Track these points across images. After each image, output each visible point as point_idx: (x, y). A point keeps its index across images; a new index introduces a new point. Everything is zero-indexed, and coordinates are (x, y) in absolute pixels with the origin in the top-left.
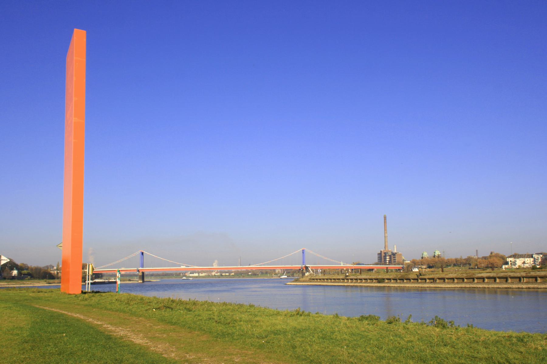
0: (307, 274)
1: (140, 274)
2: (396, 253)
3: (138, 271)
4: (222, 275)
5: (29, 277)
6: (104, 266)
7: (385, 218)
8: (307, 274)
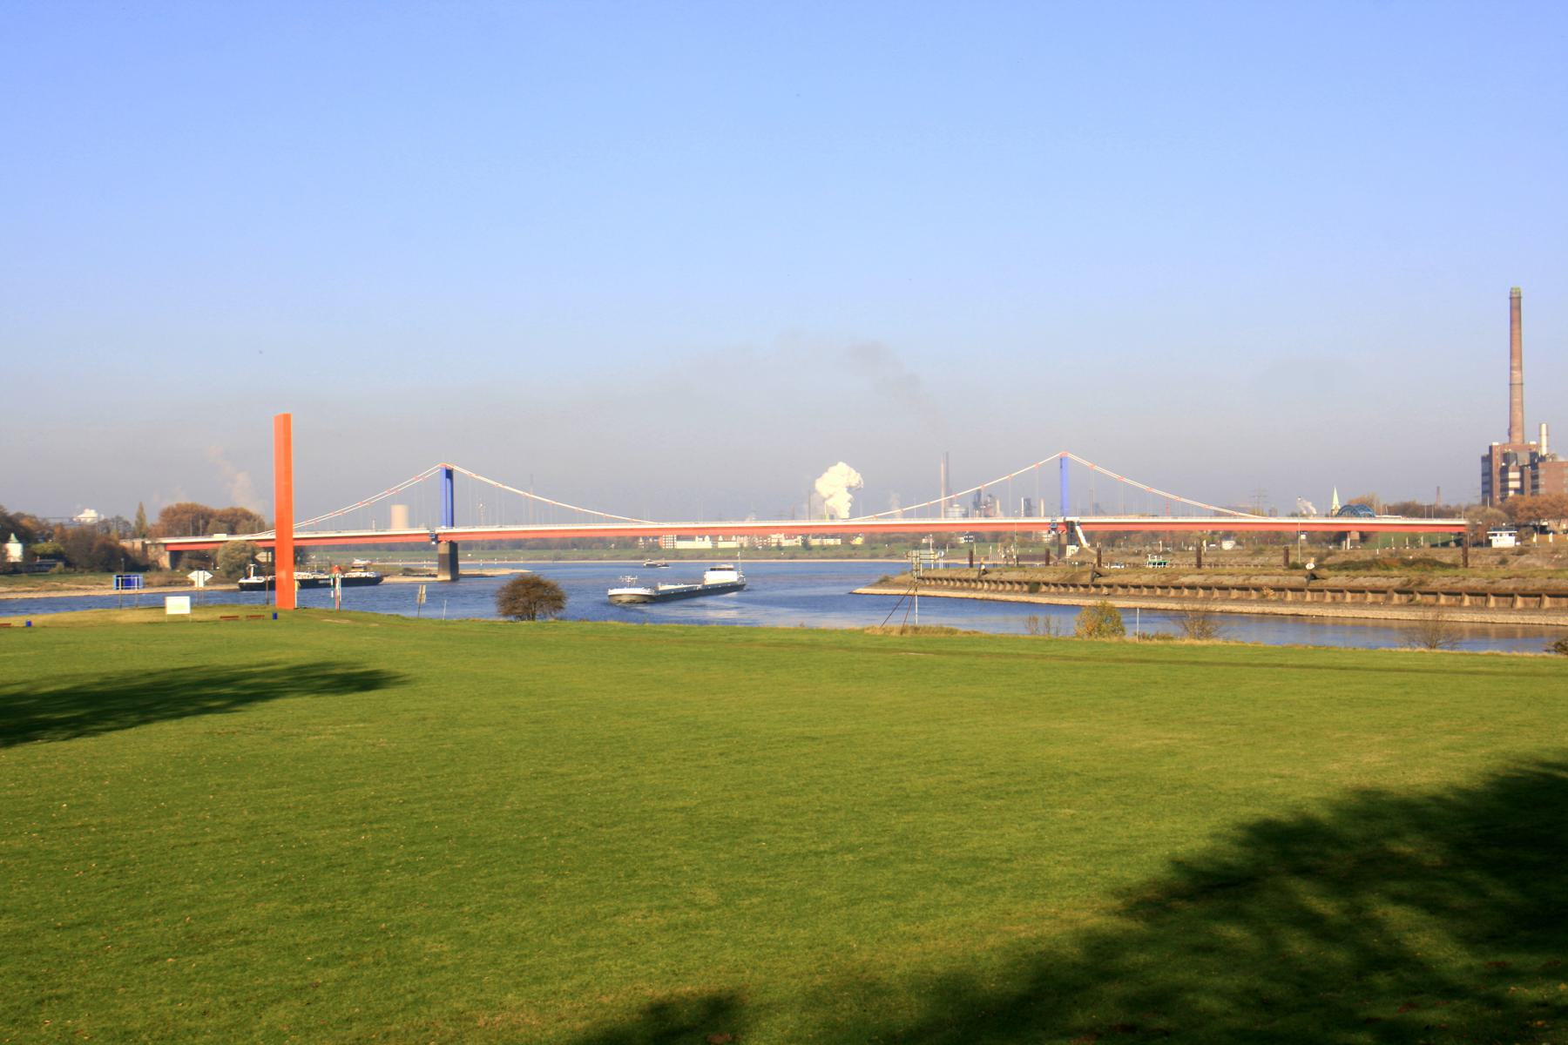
0: (1071, 550)
1: (444, 549)
2: (1543, 459)
3: (436, 538)
4: (806, 545)
5: (60, 564)
6: (311, 522)
7: (1515, 302)
8: (1071, 550)
